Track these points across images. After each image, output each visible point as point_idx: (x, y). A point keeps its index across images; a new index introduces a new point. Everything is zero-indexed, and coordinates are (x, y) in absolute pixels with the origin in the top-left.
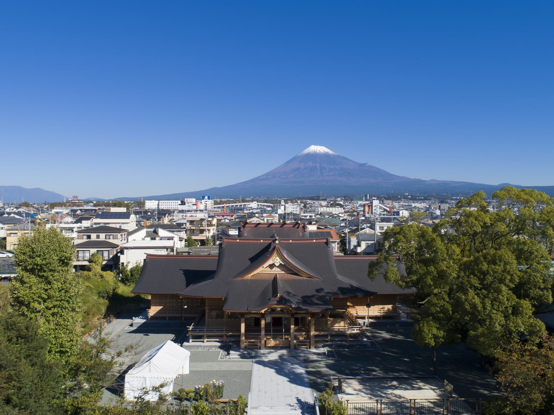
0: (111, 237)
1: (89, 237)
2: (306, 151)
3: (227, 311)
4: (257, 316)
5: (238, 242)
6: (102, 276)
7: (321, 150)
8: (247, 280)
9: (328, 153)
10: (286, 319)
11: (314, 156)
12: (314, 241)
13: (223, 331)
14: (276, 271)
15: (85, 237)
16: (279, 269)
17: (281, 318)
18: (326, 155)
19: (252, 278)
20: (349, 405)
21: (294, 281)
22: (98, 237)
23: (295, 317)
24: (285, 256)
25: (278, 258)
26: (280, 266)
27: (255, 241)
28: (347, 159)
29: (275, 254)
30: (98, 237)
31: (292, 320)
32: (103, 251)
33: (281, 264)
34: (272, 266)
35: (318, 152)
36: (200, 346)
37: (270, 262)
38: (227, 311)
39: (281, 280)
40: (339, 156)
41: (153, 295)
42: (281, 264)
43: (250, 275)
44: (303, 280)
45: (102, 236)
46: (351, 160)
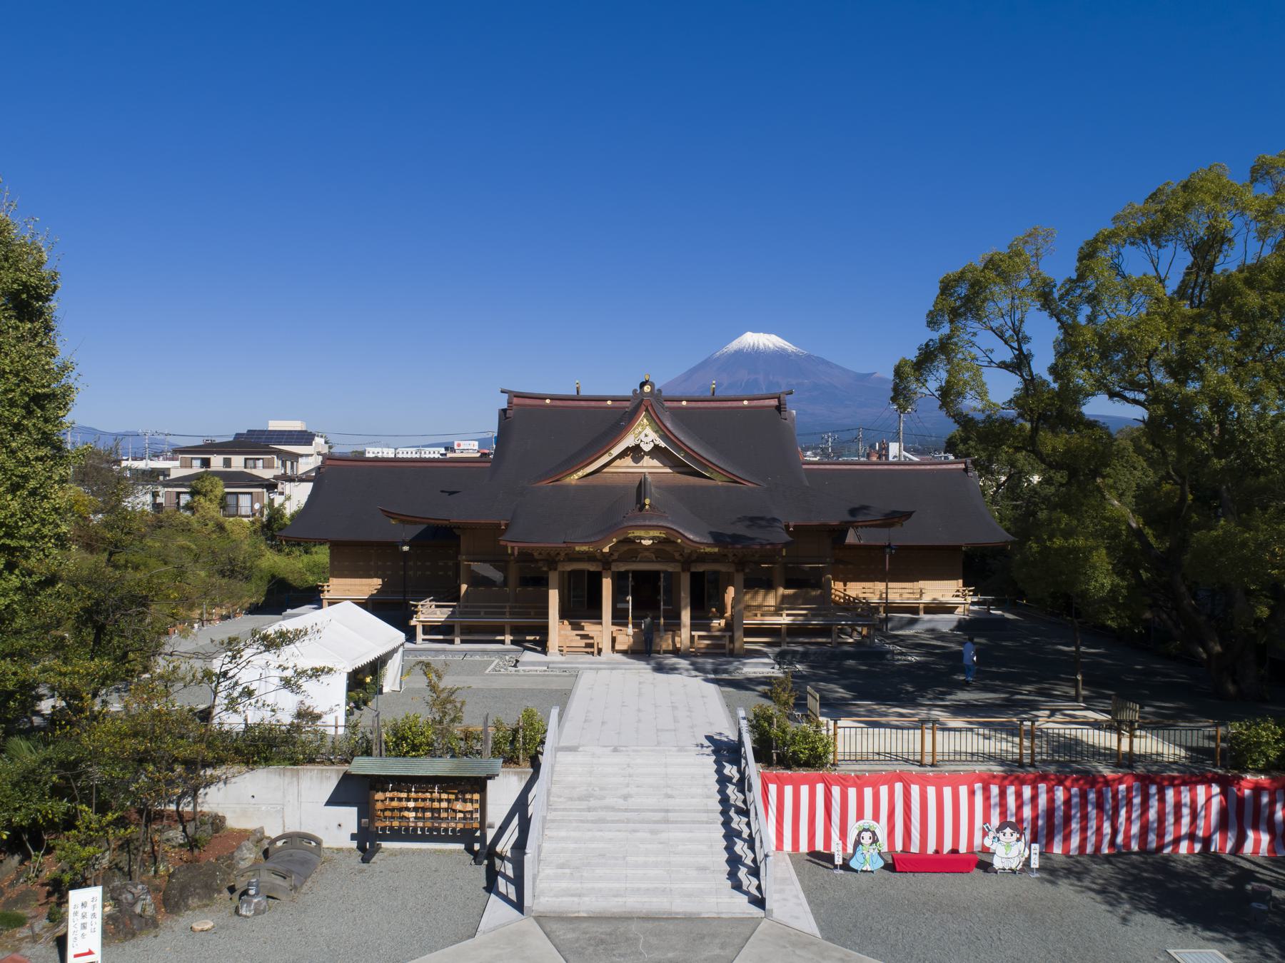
0: (260, 463)
1: (206, 463)
2: (735, 345)
3: (510, 545)
4: (592, 567)
5: (547, 406)
6: (221, 527)
7: (767, 343)
8: (568, 487)
9: (784, 350)
10: (669, 575)
11: (754, 357)
12: (746, 403)
13: (504, 613)
14: (650, 465)
15: (197, 463)
16: (655, 463)
17: (657, 573)
18: (780, 355)
19: (579, 483)
20: (840, 731)
21: (693, 488)
22: (227, 463)
23: (693, 570)
24: (669, 425)
25: (648, 431)
26: (656, 452)
27: (593, 404)
28: (827, 363)
29: (643, 420)
30: (227, 463)
31: (685, 581)
32: (237, 494)
33: (656, 447)
34: (635, 452)
35: (761, 346)
36: (444, 651)
37: (629, 441)
38: (510, 545)
39: (657, 487)
40: (809, 356)
41: (337, 547)
42: (656, 447)
43: (575, 477)
44: (717, 487)
45: (238, 462)
46: (837, 366)
